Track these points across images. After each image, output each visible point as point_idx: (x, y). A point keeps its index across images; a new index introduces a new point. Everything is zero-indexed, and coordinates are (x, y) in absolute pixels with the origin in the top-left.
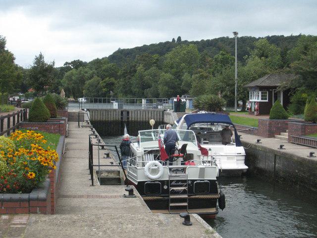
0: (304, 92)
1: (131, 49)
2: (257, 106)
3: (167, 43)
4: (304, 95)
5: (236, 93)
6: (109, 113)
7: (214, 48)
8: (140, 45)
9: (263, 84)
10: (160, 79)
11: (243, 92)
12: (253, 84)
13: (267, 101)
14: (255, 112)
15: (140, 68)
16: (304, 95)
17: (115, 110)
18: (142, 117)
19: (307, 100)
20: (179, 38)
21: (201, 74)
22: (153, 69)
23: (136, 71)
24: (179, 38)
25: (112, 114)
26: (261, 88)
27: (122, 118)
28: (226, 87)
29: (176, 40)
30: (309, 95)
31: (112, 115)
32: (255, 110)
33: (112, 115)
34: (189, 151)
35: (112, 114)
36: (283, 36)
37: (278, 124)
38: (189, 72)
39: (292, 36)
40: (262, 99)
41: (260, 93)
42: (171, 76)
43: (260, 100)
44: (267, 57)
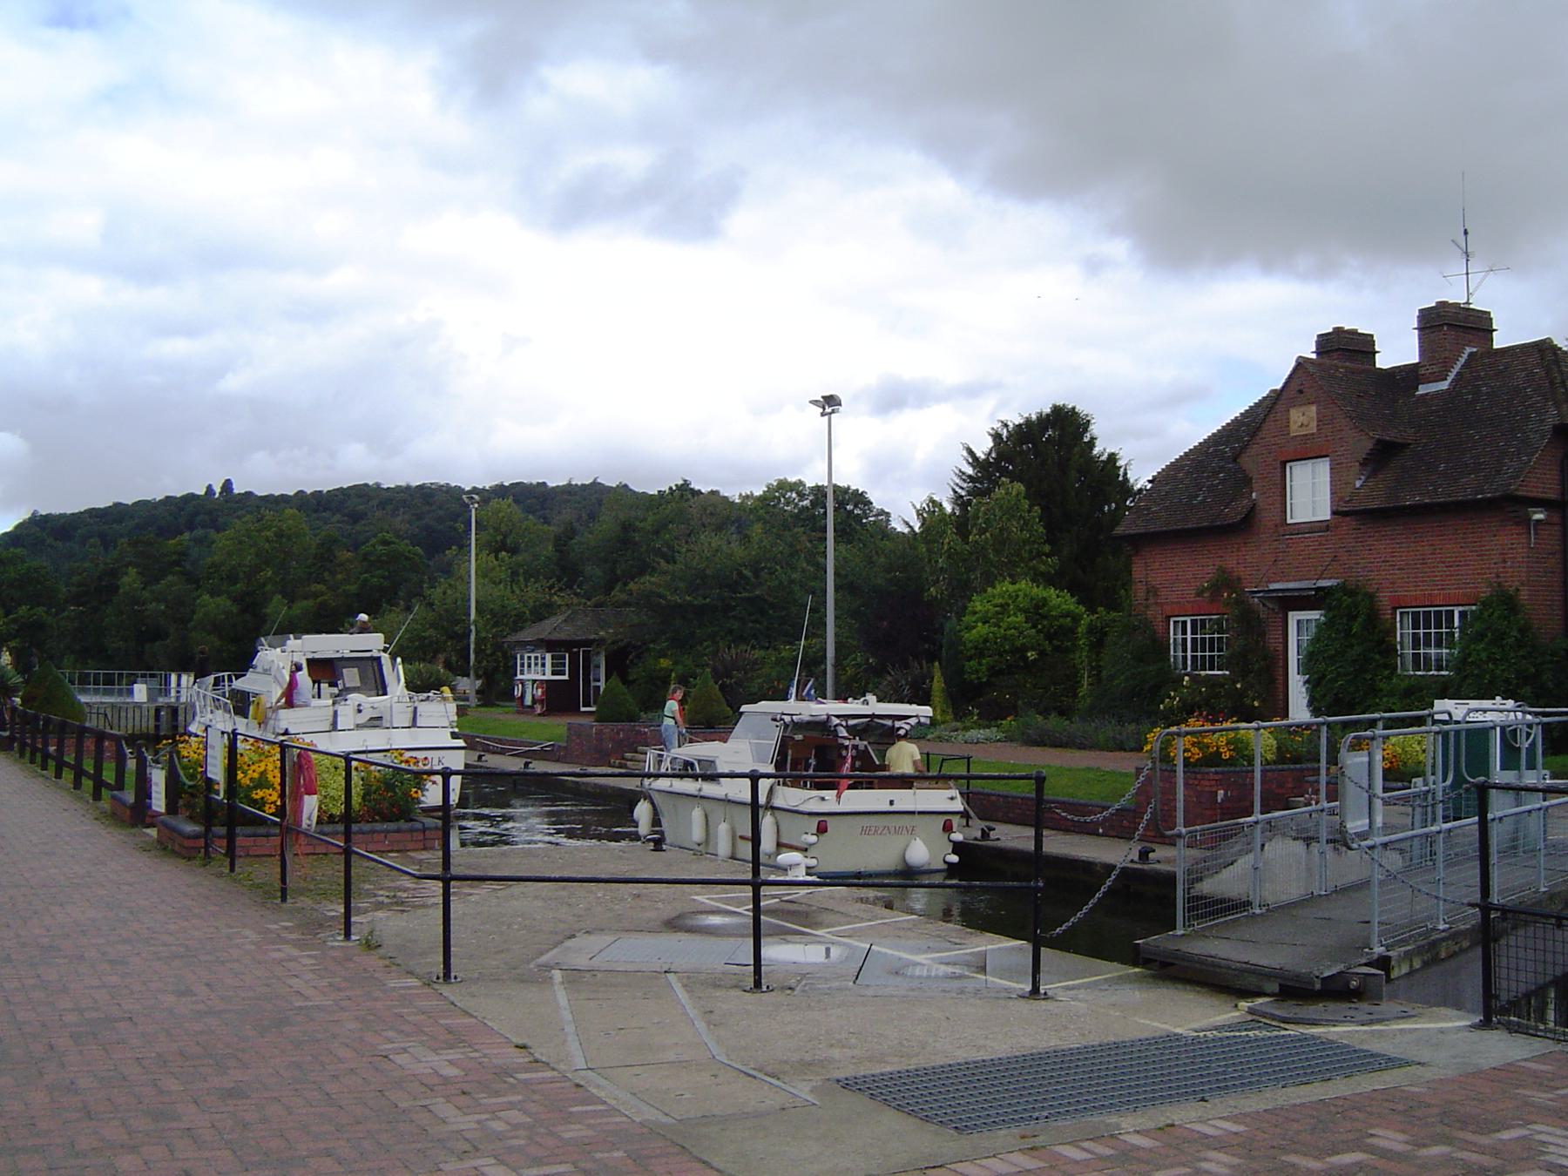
0: (665, 656)
1: (106, 508)
2: (540, 690)
3: (191, 497)
4: (664, 663)
5: (472, 657)
6: (123, 714)
7: (338, 517)
8: (103, 502)
9: (556, 636)
10: (193, 612)
11: (492, 654)
12: (527, 635)
13: (566, 677)
14: (538, 709)
15: (130, 579)
16: (664, 663)
17: (138, 706)
18: (144, 725)
19: (673, 675)
20: (227, 485)
21: (319, 600)
22: (171, 583)
23: (118, 588)
24: (227, 485)
25: (130, 715)
26: (550, 645)
27: (157, 727)
28: (445, 642)
29: (218, 490)
30: (676, 663)
31: (130, 721)
32: (534, 701)
33: (130, 721)
34: (1352, 828)
35: (130, 715)
36: (301, 491)
37: (618, 733)
38: (285, 594)
39: (569, 485)
40: (553, 674)
41: (548, 656)
42: (229, 603)
43: (549, 676)
44: (514, 551)
